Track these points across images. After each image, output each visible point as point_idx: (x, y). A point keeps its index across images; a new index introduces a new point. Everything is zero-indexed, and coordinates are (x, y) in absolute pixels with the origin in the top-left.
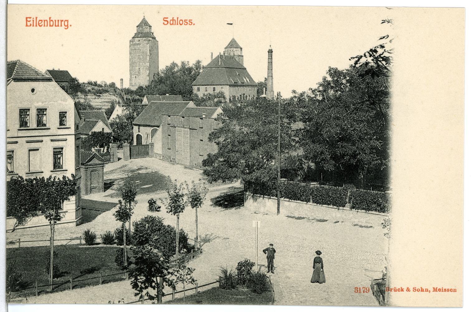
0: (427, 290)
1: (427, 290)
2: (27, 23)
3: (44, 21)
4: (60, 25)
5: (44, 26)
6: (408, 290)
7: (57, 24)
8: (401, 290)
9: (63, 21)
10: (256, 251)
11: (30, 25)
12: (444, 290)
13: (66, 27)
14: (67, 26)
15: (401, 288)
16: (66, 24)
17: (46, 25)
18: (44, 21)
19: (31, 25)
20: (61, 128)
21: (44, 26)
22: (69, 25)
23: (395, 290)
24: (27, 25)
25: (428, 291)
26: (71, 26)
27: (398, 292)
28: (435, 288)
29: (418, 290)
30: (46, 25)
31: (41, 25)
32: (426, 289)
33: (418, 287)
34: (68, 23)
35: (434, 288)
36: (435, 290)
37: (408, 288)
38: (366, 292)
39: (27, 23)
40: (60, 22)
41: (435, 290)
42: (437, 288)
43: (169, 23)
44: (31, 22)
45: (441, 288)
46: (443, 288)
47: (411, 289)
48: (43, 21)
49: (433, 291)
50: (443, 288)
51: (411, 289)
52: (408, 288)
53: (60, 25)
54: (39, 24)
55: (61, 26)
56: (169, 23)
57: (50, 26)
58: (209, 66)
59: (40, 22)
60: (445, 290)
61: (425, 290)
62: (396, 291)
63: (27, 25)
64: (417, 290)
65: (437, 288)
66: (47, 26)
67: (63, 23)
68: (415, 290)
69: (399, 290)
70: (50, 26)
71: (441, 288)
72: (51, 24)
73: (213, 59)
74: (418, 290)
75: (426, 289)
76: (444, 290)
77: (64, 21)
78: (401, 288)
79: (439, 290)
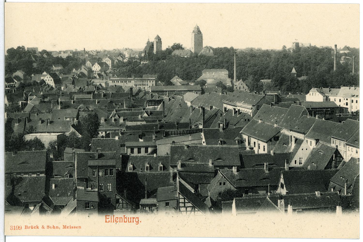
0: (57, 227)
1: (57, 227)
2: (106, 220)
3: (120, 218)
4: (132, 221)
5: (120, 222)
6: (43, 227)
7: (130, 221)
8: (36, 228)
9: (134, 218)
11: (108, 221)
13: (137, 223)
14: (138, 222)
15: (37, 226)
16: (137, 221)
17: (121, 221)
18: (120, 218)
19: (109, 221)
21: (120, 222)
22: (139, 222)
23: (32, 227)
24: (106, 222)
26: (141, 222)
28: (65, 226)
30: (121, 221)
31: (117, 221)
32: (57, 227)
33: (51, 225)
34: (138, 219)
35: (64, 226)
36: (65, 227)
37: (43, 226)
39: (106, 220)
40: (132, 219)
41: (65, 227)
44: (110, 219)
47: (46, 227)
49: (63, 228)
50: (66, 226)
51: (46, 227)
52: (43, 226)
53: (132, 221)
54: (115, 220)
55: (133, 222)
57: (124, 222)
59: (117, 219)
61: (56, 228)
63: (106, 222)
64: (76, 227)
66: (122, 222)
67: (134, 219)
68: (48, 228)
69: (35, 228)
70: (124, 222)
72: (125, 221)
76: (71, 227)
77: (135, 218)
78: (37, 226)
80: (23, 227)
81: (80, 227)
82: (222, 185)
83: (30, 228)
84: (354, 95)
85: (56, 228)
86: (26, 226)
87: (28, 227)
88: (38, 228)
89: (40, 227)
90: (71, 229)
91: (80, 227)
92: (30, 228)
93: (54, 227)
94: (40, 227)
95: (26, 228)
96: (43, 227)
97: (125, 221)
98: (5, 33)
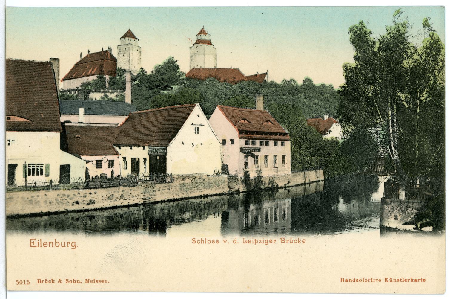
0: (78, 281)
1: (78, 281)
6: (60, 281)
7: (63, 245)
8: (51, 282)
10: (211, 127)
12: (95, 282)
13: (74, 247)
15: (52, 279)
20: (103, 124)
25: (79, 282)
27: (359, 282)
29: (71, 282)
32: (77, 281)
35: (86, 280)
36: (87, 281)
38: (27, 284)
41: (87, 281)
42: (89, 280)
43: (60, 245)
45: (93, 280)
46: (363, 278)
47: (64, 281)
48: (48, 243)
51: (64, 281)
54: (44, 245)
56: (60, 245)
58: (347, 83)
60: (97, 281)
61: (76, 282)
62: (47, 283)
65: (89, 280)
68: (67, 282)
69: (50, 282)
71: (93, 280)
73: (83, 57)
74: (360, 280)
75: (77, 281)
78: (52, 279)
79: (91, 281)
83: (375, 281)
85: (76, 282)
86: (38, 280)
87: (42, 281)
88: (53, 282)
89: (56, 281)
92: (375, 281)
93: (74, 281)
94: (80, 282)
95: (38, 283)
96: (60, 281)
97: (51, 243)
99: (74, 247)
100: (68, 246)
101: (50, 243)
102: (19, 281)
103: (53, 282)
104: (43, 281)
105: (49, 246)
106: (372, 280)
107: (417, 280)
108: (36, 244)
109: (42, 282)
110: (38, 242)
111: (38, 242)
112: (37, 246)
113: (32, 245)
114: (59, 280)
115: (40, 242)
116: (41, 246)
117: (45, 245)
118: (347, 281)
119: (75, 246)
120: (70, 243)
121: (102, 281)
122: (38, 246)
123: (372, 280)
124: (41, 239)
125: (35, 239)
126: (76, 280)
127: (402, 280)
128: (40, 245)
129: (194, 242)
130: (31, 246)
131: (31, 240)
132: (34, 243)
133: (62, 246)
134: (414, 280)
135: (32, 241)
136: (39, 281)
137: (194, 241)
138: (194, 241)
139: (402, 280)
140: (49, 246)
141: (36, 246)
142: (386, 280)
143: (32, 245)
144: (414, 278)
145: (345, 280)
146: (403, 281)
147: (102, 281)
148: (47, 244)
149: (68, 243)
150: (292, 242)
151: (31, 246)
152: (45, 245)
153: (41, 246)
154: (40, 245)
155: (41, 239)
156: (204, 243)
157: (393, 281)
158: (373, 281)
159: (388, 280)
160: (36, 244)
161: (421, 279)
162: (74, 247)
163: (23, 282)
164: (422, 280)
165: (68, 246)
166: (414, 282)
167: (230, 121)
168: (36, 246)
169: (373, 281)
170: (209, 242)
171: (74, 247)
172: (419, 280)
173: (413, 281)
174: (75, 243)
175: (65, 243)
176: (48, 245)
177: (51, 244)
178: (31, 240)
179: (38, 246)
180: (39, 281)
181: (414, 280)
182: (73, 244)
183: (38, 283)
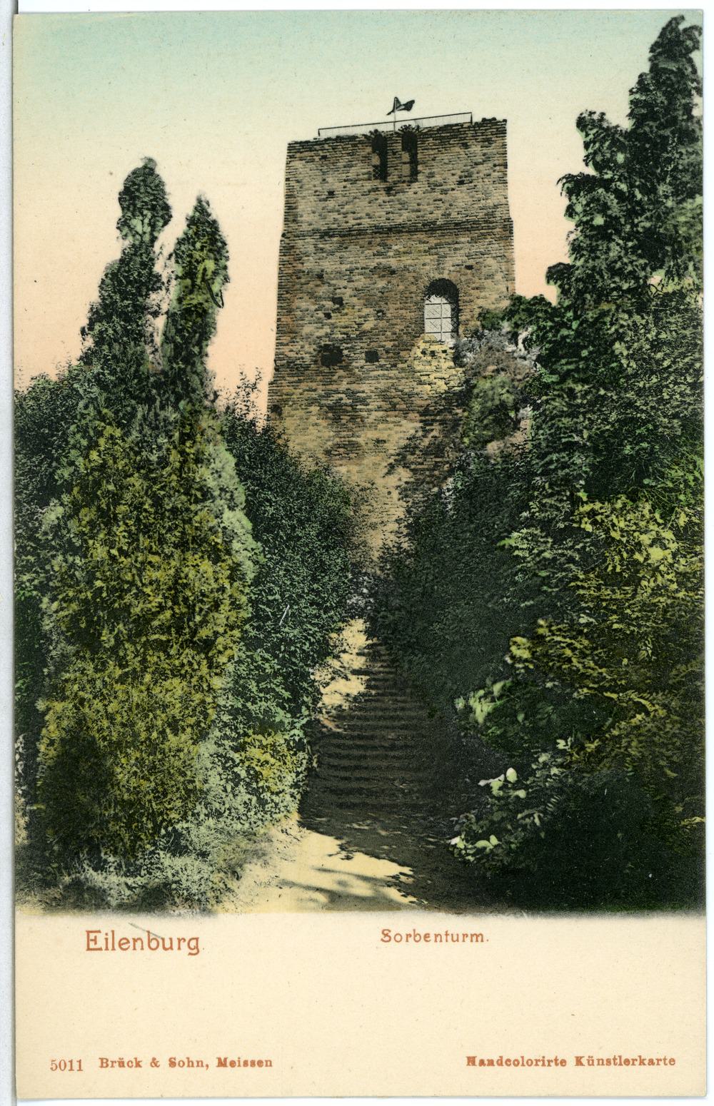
0: (200, 1064)
1: (200, 1064)
6: (154, 1063)
7: (168, 945)
13: (195, 951)
29: (182, 1064)
32: (599, 1060)
35: (219, 1059)
36: (222, 1063)
41: (222, 1063)
42: (225, 1059)
47: (164, 1062)
48: (131, 941)
51: (164, 1062)
61: (195, 1064)
65: (225, 1059)
80: (571, 1062)
81: (269, 1064)
82: (443, 933)
83: (553, 1064)
84: (427, 936)
85: (195, 1064)
86: (102, 1059)
87: (110, 1063)
88: (138, 1065)
89: (146, 1062)
90: (242, 1068)
91: (672, 1061)
92: (553, 1064)
93: (190, 1064)
94: (146, 1062)
95: (102, 1067)
97: (139, 942)
98: (382, 1097)
99: (195, 951)
100: (179, 948)
101: (135, 941)
102: (57, 1063)
103: (138, 1065)
104: (549, 1061)
105: (135, 949)
106: (544, 1062)
107: (655, 1061)
108: (101, 943)
109: (110, 1063)
110: (107, 939)
111: (107, 939)
112: (104, 948)
113: (92, 945)
114: (154, 1059)
115: (110, 937)
116: (113, 949)
117: (124, 947)
118: (482, 1063)
119: (197, 947)
120: (184, 940)
121: (260, 1063)
122: (107, 949)
123: (544, 1062)
124: (113, 932)
125: (99, 932)
126: (194, 1059)
127: (618, 1061)
128: (110, 946)
129: (387, 938)
130: (89, 949)
131: (88, 932)
132: (95, 940)
133: (165, 949)
134: (646, 1062)
135: (92, 936)
136: (104, 1063)
137: (386, 935)
138: (386, 934)
139: (618, 1061)
140: (135, 949)
141: (100, 949)
142: (579, 1061)
143: (92, 945)
144: (647, 1056)
145: (477, 1062)
146: (621, 1064)
147: (260, 1063)
148: (128, 942)
149: (179, 940)
150: (171, 948)
151: (89, 949)
152: (124, 947)
153: (113, 949)
154: (110, 946)
155: (113, 932)
156: (142, 949)
157: (596, 1062)
158: (546, 1063)
159: (584, 1061)
160: (101, 943)
161: (556, 1060)
162: (195, 951)
163: (68, 1064)
164: (667, 1062)
165: (179, 948)
166: (647, 1068)
167: (373, 12)
168: (100, 949)
169: (546, 1063)
170: (398, 938)
171: (195, 951)
172: (658, 1060)
173: (582, 1064)
174: (197, 939)
175: (171, 939)
176: (131, 944)
177: (138, 944)
178: (88, 932)
179: (107, 949)
180: (104, 1063)
181: (646, 1062)
182: (193, 944)
183: (102, 1067)
